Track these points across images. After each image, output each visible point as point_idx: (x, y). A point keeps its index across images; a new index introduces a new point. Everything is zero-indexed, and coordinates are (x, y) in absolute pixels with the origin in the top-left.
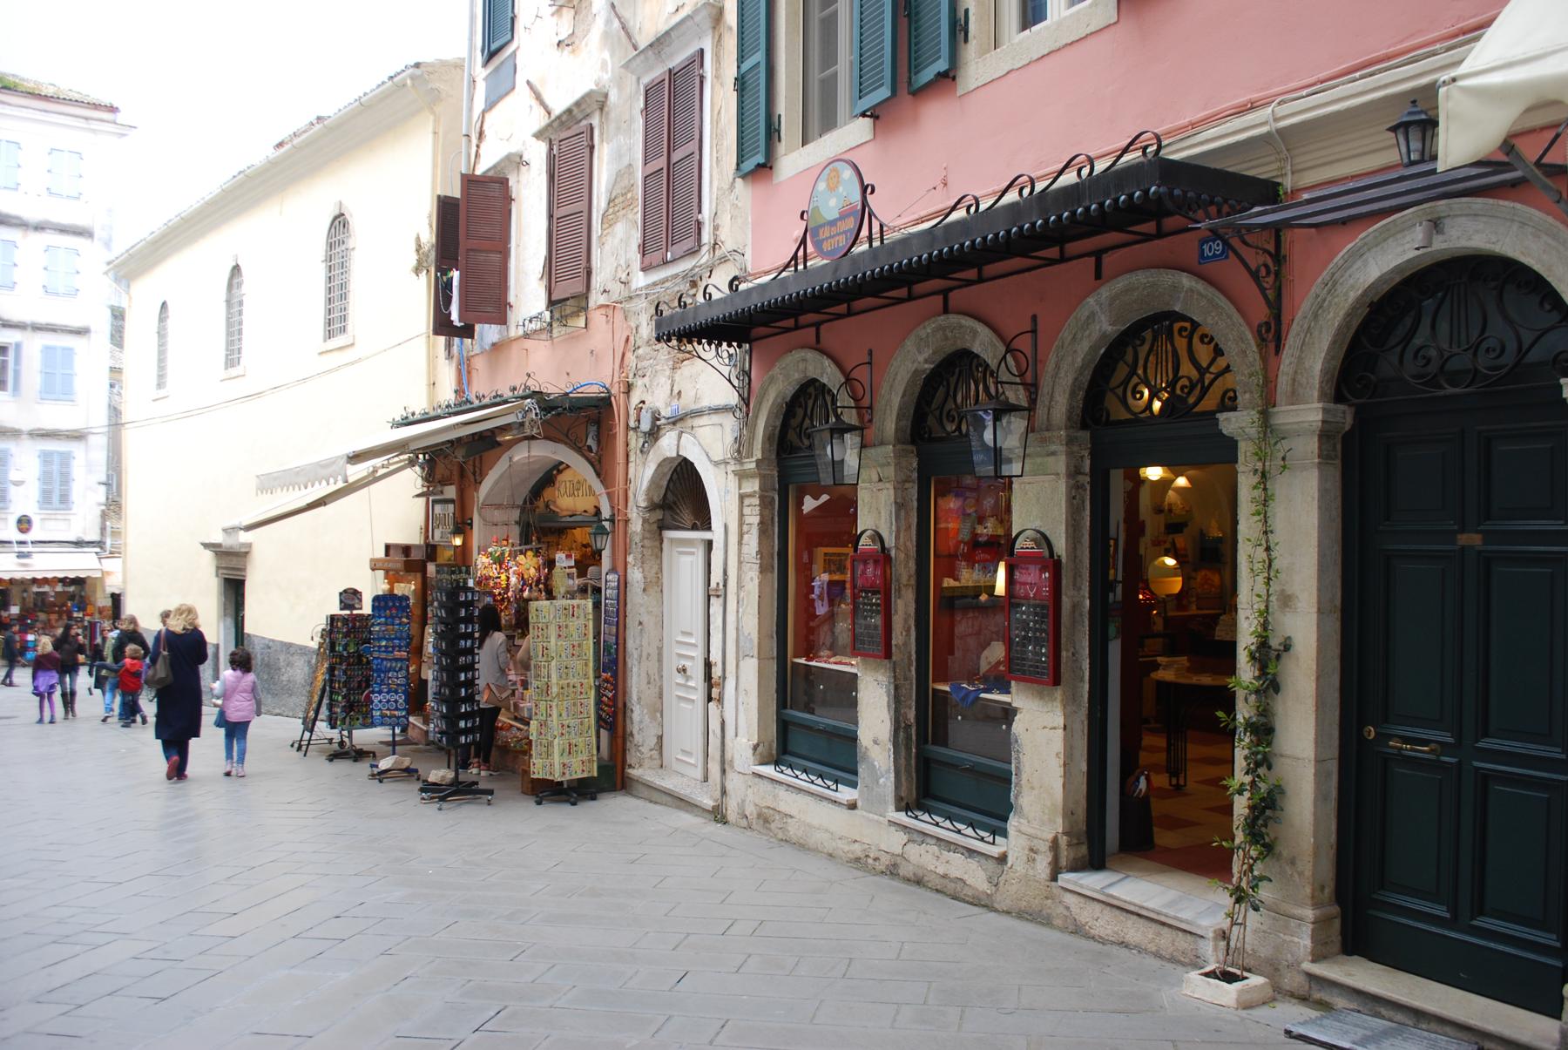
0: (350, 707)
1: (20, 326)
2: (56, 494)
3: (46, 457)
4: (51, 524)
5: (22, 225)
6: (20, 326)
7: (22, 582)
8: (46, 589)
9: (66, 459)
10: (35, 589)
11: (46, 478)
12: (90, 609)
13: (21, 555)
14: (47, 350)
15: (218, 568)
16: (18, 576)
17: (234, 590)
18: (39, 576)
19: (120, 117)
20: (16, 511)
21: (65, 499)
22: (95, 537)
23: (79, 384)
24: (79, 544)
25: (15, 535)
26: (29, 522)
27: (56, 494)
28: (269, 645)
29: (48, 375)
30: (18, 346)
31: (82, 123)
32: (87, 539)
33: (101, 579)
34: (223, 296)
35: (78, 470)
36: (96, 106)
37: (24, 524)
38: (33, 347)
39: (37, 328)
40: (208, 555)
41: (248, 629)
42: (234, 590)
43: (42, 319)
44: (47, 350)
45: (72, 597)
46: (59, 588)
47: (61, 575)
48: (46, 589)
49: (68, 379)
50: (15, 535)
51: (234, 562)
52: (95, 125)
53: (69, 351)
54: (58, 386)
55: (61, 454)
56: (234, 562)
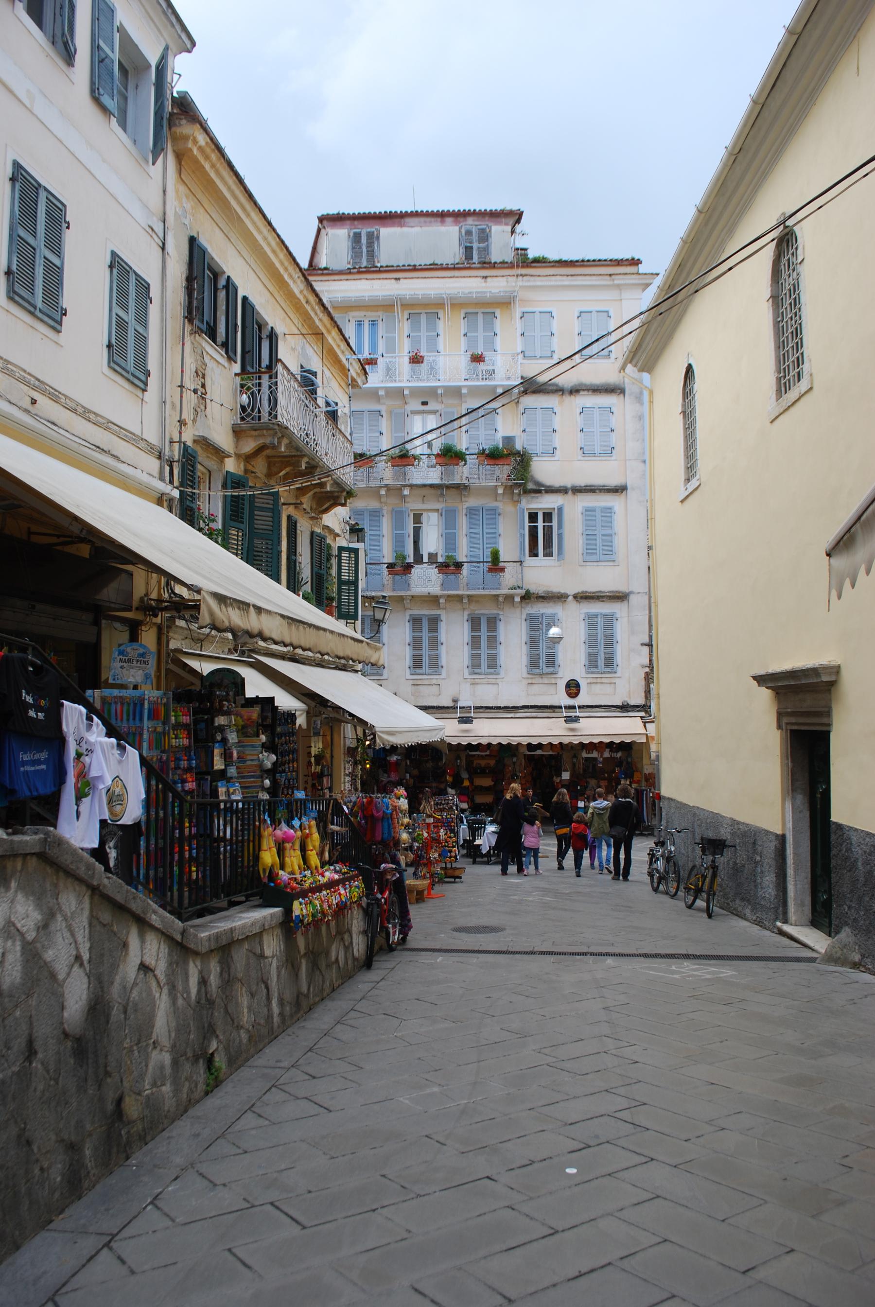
0: (237, 502)
1: (562, 490)
2: (601, 658)
3: (591, 621)
4: (597, 688)
5: (560, 391)
6: (562, 490)
7: (570, 747)
8: (595, 754)
9: (610, 621)
10: (584, 755)
11: (591, 641)
12: (636, 776)
13: (569, 720)
14: (589, 512)
15: (780, 715)
16: (566, 741)
17: (808, 753)
18: (586, 741)
19: (642, 268)
20: (565, 674)
21: (610, 662)
22: (640, 700)
23: (619, 542)
24: (625, 708)
25: (564, 700)
26: (578, 686)
27: (601, 658)
28: (840, 826)
29: (590, 537)
30: (560, 510)
31: (606, 281)
32: (632, 703)
33: (647, 745)
34: (766, 291)
35: (621, 631)
36: (618, 263)
37: (573, 688)
38: (574, 510)
39: (577, 490)
40: (765, 695)
41: (840, 812)
42: (808, 753)
43: (581, 482)
44: (589, 512)
45: (619, 763)
46: (607, 754)
47: (607, 740)
48: (595, 754)
49: (609, 538)
50: (564, 700)
51: (808, 702)
52: (618, 281)
53: (608, 511)
54: (600, 547)
55: (605, 616)
56: (808, 702)
